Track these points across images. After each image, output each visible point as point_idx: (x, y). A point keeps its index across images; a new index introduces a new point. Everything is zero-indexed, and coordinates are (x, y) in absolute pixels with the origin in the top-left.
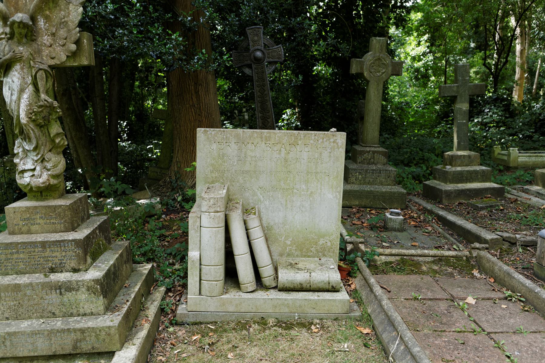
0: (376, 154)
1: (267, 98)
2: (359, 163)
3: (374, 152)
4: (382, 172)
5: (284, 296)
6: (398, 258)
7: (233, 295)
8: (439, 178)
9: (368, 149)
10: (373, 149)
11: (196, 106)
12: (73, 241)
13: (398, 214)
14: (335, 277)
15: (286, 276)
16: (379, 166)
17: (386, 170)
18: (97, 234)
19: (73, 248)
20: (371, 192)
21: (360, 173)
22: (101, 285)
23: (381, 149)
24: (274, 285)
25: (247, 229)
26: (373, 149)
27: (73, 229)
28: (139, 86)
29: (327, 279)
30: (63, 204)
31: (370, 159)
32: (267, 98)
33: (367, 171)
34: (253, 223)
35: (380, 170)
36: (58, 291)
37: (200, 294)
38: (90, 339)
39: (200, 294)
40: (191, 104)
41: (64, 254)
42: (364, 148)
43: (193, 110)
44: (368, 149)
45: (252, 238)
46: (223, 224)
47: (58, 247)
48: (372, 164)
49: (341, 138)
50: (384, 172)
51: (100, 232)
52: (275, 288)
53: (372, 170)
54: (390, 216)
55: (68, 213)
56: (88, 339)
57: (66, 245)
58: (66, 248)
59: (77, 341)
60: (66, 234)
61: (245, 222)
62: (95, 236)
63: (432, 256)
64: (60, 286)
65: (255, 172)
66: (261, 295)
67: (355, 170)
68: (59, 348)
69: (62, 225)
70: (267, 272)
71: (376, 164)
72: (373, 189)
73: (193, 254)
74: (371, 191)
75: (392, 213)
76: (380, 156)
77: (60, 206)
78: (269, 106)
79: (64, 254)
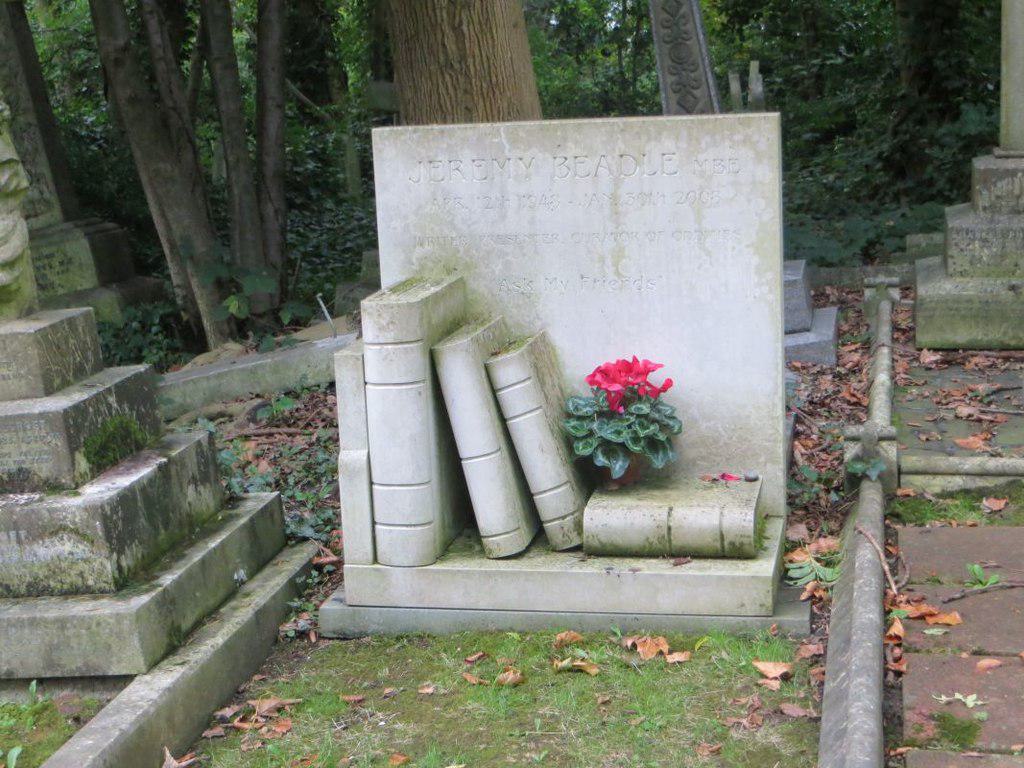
1: (689, 27)
6: (1002, 480)
11: (457, 66)
12: (42, 415)
18: (110, 407)
19: (43, 433)
21: (985, 241)
22: (105, 519)
25: (494, 391)
27: (49, 392)
28: (924, 149)
29: (717, 522)
30: (23, 331)
32: (689, 27)
33: (1004, 234)
34: (511, 371)
36: (13, 534)
37: (375, 560)
38: (79, 644)
40: (442, 59)
41: (24, 448)
43: (447, 77)
44: (1011, 164)
45: (508, 413)
46: (427, 375)
47: (9, 431)
51: (120, 402)
52: (578, 549)
55: (33, 352)
56: (74, 643)
57: (28, 427)
58: (29, 433)
59: (52, 648)
60: (30, 402)
61: (487, 368)
62: (103, 408)
63: (551, 362)
64: (15, 523)
65: (532, 236)
66: (539, 564)
68: (15, 663)
69: (23, 382)
73: (350, 455)
77: (15, 335)
78: (696, 50)
79: (24, 448)
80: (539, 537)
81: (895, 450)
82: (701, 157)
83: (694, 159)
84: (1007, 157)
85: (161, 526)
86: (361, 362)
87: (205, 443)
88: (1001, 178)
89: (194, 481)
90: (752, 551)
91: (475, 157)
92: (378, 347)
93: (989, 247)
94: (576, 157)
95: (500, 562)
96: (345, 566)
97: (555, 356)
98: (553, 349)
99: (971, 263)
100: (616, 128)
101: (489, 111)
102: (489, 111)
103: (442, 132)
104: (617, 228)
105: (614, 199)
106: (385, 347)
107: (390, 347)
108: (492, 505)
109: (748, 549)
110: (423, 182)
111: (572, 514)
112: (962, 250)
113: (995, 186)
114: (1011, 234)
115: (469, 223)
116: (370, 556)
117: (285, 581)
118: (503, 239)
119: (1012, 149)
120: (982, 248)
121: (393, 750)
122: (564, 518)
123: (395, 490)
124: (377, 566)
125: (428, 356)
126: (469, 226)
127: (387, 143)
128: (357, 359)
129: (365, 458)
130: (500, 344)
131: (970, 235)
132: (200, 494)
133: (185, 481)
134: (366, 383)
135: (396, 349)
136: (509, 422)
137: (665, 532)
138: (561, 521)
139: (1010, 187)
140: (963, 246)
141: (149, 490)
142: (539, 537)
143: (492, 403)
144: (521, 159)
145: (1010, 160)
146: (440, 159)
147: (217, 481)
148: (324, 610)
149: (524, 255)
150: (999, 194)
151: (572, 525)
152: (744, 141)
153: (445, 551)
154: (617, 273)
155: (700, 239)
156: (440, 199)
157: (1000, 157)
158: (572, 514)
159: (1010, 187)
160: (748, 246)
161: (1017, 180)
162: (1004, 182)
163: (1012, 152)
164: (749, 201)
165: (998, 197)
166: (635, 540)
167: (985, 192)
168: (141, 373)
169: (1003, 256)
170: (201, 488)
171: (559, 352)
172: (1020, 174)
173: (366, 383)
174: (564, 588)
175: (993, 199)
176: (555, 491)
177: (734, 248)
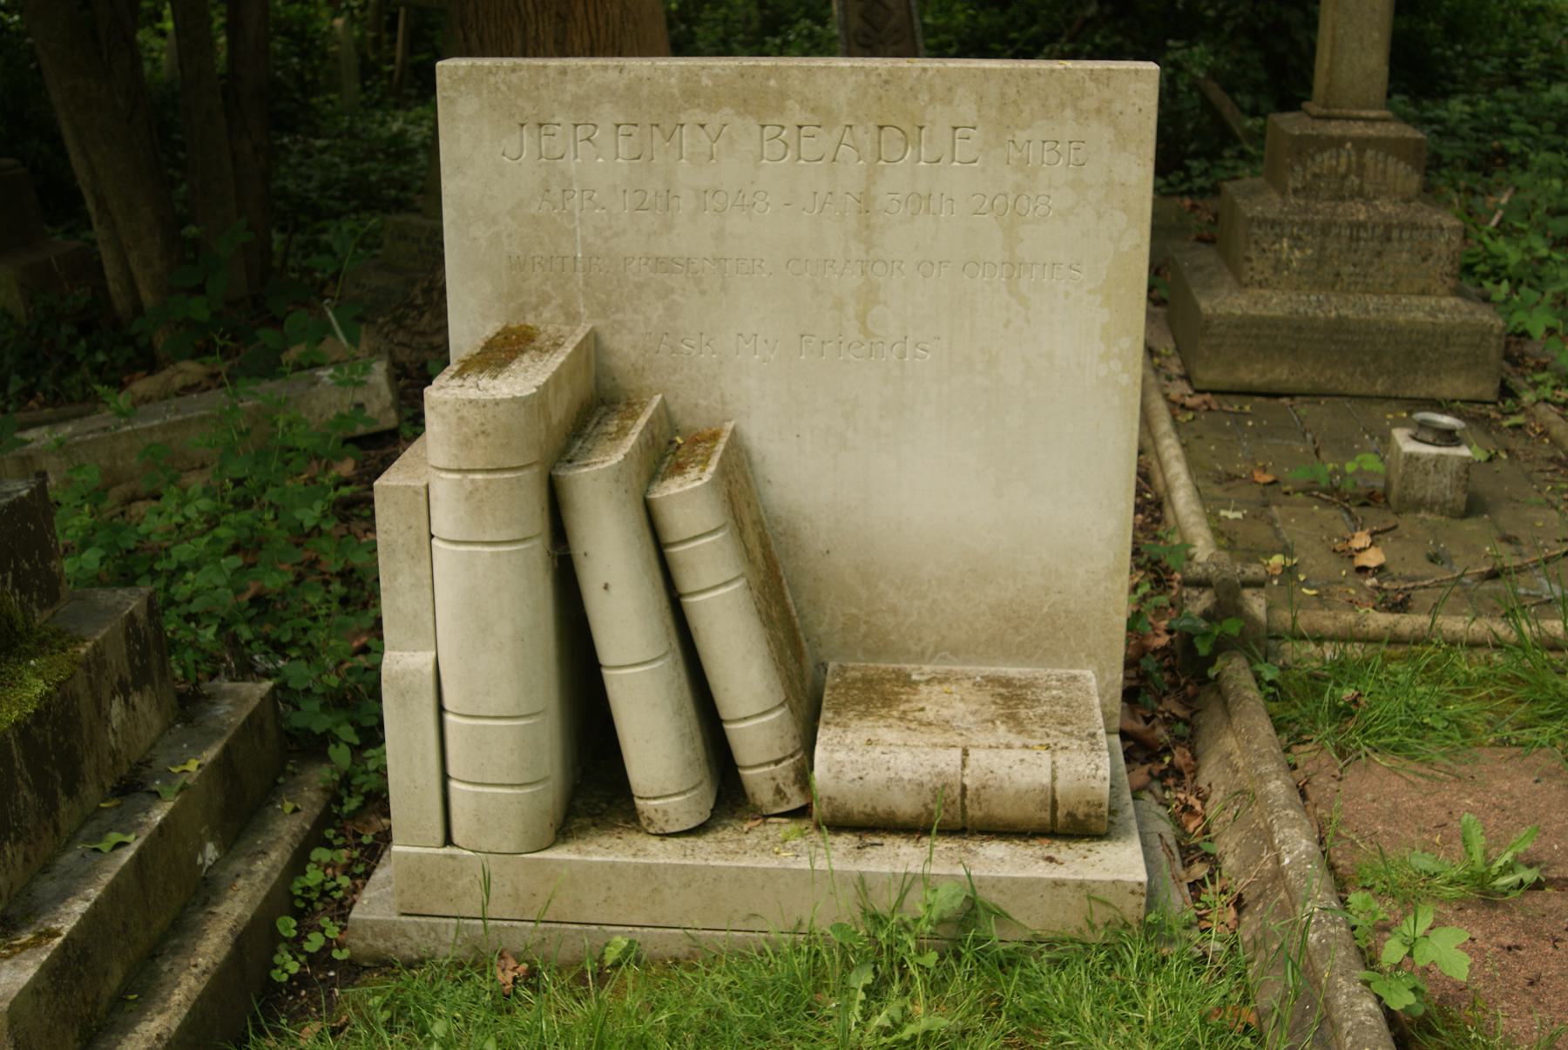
0: (1370, 153)
2: (1296, 191)
3: (1362, 144)
4: (1395, 234)
5: (839, 856)
7: (601, 852)
8: (365, 650)
9: (1335, 129)
10: (1357, 129)
13: (1448, 437)
14: (1089, 767)
15: (855, 757)
16: (1387, 207)
17: (1414, 226)
20: (1340, 325)
23: (1396, 130)
24: (797, 802)
26: (1357, 129)
31: (1344, 177)
33: (1326, 229)
34: (687, 497)
35: (1389, 228)
37: (448, 840)
39: (448, 840)
42: (1318, 123)
44: (1335, 129)
45: (686, 583)
48: (1352, 197)
49: (1135, 85)
50: (1406, 235)
52: (801, 813)
53: (1351, 225)
54: (1411, 447)
67: (1273, 224)
70: (757, 732)
71: (1368, 200)
72: (1348, 312)
73: (402, 662)
74: (1341, 320)
75: (1424, 432)
76: (1391, 160)
80: (728, 794)
81: (1262, 602)
82: (1021, 136)
83: (1010, 137)
84: (1329, 118)
85: (60, 791)
86: (423, 499)
87: (142, 616)
88: (1321, 150)
89: (123, 689)
90: (1104, 829)
91: (621, 120)
92: (457, 476)
93: (1301, 249)
94: (800, 127)
95: (670, 843)
96: (395, 848)
97: (750, 464)
98: (748, 453)
99: (1276, 269)
100: (873, 79)
101: (592, 20)
102: (592, 20)
103: (563, 72)
104: (867, 252)
105: (866, 203)
106: (471, 476)
107: (479, 476)
108: (654, 748)
109: (1095, 825)
110: (532, 163)
111: (792, 756)
112: (1264, 251)
113: (1313, 160)
114: (1334, 231)
115: (608, 233)
116: (439, 835)
117: (288, 857)
118: (664, 264)
119: (1335, 107)
120: (1291, 248)
121: (326, 157)
122: (777, 762)
123: (485, 727)
124: (448, 850)
125: (545, 489)
126: (606, 240)
127: (463, 88)
128: (416, 493)
129: (430, 668)
130: (666, 452)
131: (1277, 230)
132: (134, 708)
133: (106, 694)
134: (432, 536)
135: (490, 481)
136: (687, 601)
137: (958, 791)
138: (773, 767)
139: (1334, 162)
140: (1265, 246)
141: (35, 730)
142: (728, 794)
143: (655, 563)
144: (702, 126)
145: (1333, 123)
146: (557, 120)
147: (164, 671)
148: (355, 921)
149: (703, 293)
150: (1317, 171)
151: (792, 775)
152: (1098, 111)
153: (566, 827)
154: (864, 330)
155: (1010, 277)
156: (556, 190)
157: (1319, 117)
158: (792, 756)
159: (1334, 162)
160: (1090, 292)
161: (1344, 154)
162: (1326, 155)
163: (1336, 112)
164: (1100, 216)
165: (1315, 176)
166: (906, 806)
167: (1298, 168)
168: (22, 499)
169: (1320, 262)
170: (136, 698)
171: (756, 458)
172: (1349, 145)
173: (432, 536)
174: (782, 876)
175: (1308, 177)
176: (764, 719)
177: (1067, 294)
